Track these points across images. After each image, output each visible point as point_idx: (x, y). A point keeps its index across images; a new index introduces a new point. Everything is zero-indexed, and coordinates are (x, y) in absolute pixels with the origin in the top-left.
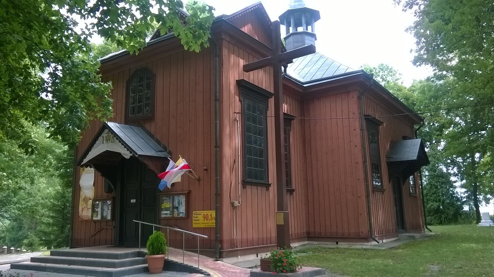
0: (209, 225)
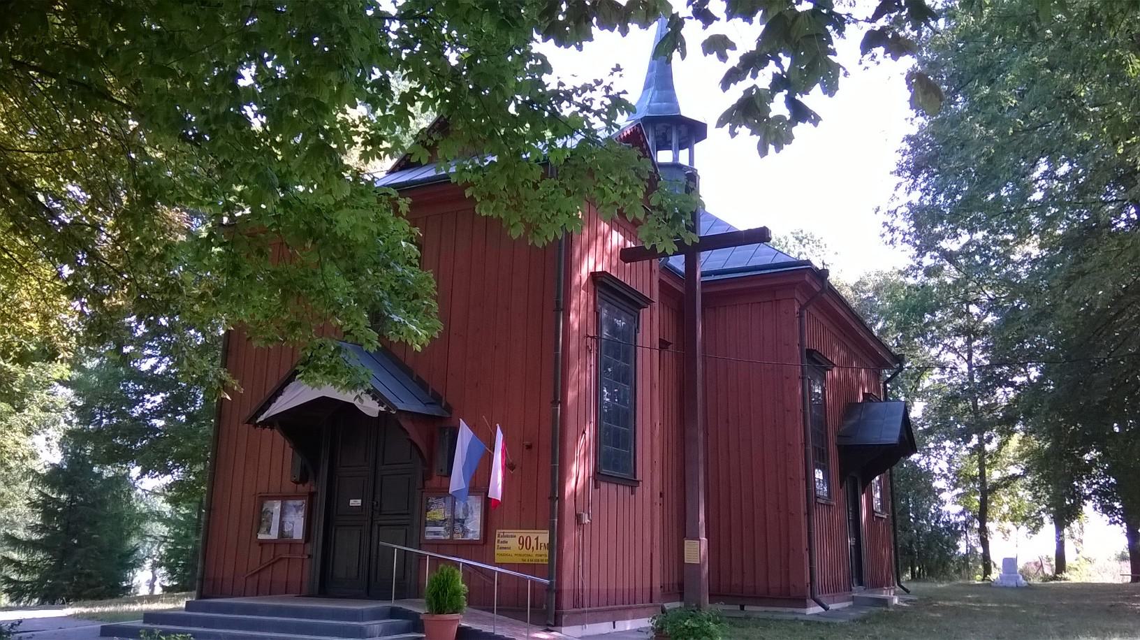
0: (532, 558)
